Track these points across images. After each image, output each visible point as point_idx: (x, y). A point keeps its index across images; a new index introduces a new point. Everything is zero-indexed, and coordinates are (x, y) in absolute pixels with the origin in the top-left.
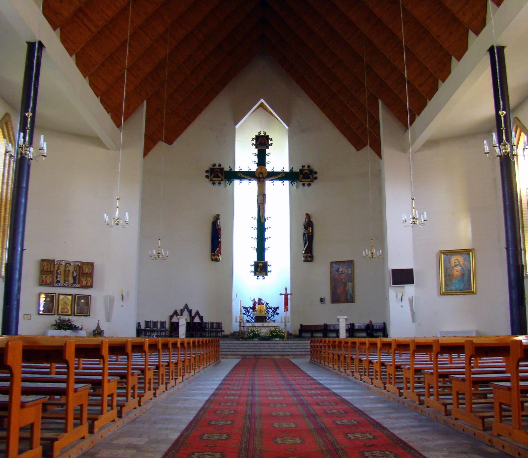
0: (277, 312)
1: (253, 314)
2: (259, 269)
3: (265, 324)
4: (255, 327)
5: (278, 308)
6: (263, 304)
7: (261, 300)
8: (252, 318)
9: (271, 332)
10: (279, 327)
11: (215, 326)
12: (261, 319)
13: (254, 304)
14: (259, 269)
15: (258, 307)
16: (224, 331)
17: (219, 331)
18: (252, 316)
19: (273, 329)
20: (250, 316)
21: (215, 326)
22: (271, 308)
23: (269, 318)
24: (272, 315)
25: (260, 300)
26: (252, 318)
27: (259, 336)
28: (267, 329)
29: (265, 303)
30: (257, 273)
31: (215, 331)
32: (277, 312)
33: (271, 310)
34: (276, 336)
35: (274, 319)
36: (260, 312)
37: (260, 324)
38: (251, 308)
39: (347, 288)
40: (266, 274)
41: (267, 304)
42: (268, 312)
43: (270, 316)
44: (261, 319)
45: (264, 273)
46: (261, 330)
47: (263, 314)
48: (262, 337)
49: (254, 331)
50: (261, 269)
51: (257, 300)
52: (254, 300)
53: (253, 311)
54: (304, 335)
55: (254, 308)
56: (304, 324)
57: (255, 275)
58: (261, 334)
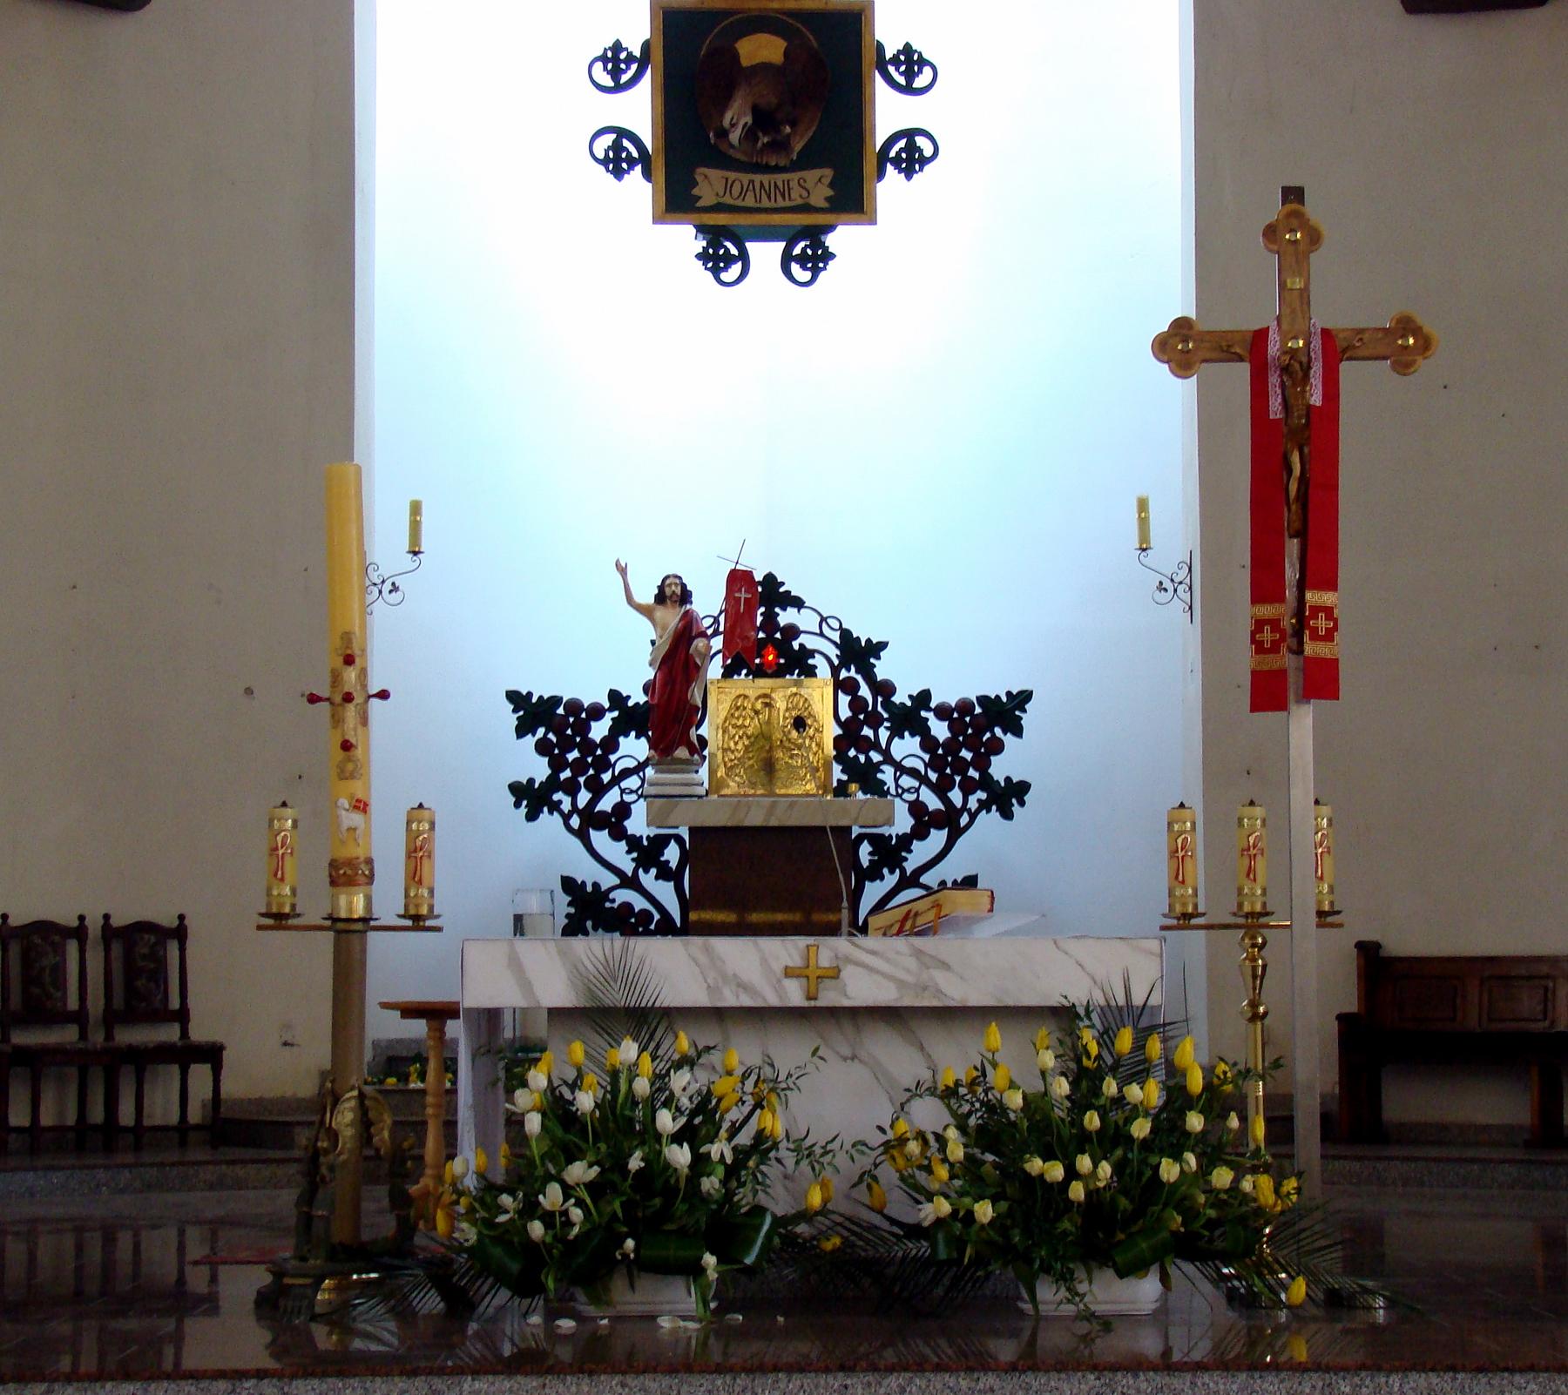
0: (1000, 768)
1: (661, 801)
2: (737, 117)
3: (870, 969)
4: (646, 1020)
5: (1005, 713)
6: (800, 663)
7: (773, 594)
8: (648, 853)
9: (998, 1135)
10: (1143, 1021)
11: (85, 976)
12: (769, 875)
13: (678, 661)
14: (737, 117)
15: (724, 698)
16: (212, 1054)
17: (144, 1059)
18: (637, 824)
19: (1026, 1071)
20: (615, 822)
21: (85, 976)
22: (908, 719)
23: (890, 852)
24: (924, 821)
25: (758, 596)
26: (648, 853)
27: (727, 1228)
28: (900, 1059)
29: (826, 649)
30: (710, 184)
31: (79, 1059)
32: (1000, 768)
33: (907, 748)
34: (1111, 1233)
35: (951, 870)
36: (765, 780)
37: (755, 966)
38: (629, 719)
39: (916, 845)
40: (853, 201)
41: (858, 653)
42: (866, 777)
43: (903, 822)
44: (769, 875)
45: (817, 184)
46: (767, 1090)
47: (804, 793)
48: (789, 1242)
49: (622, 1122)
50: (763, 120)
51: (708, 602)
52: (673, 594)
53: (663, 748)
54: (1408, 1100)
55: (667, 715)
56: (1409, 939)
57: (676, 202)
58: (780, 1192)
